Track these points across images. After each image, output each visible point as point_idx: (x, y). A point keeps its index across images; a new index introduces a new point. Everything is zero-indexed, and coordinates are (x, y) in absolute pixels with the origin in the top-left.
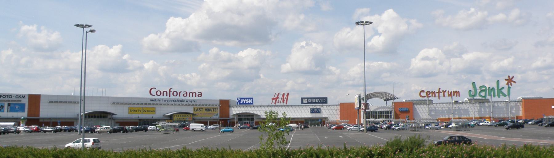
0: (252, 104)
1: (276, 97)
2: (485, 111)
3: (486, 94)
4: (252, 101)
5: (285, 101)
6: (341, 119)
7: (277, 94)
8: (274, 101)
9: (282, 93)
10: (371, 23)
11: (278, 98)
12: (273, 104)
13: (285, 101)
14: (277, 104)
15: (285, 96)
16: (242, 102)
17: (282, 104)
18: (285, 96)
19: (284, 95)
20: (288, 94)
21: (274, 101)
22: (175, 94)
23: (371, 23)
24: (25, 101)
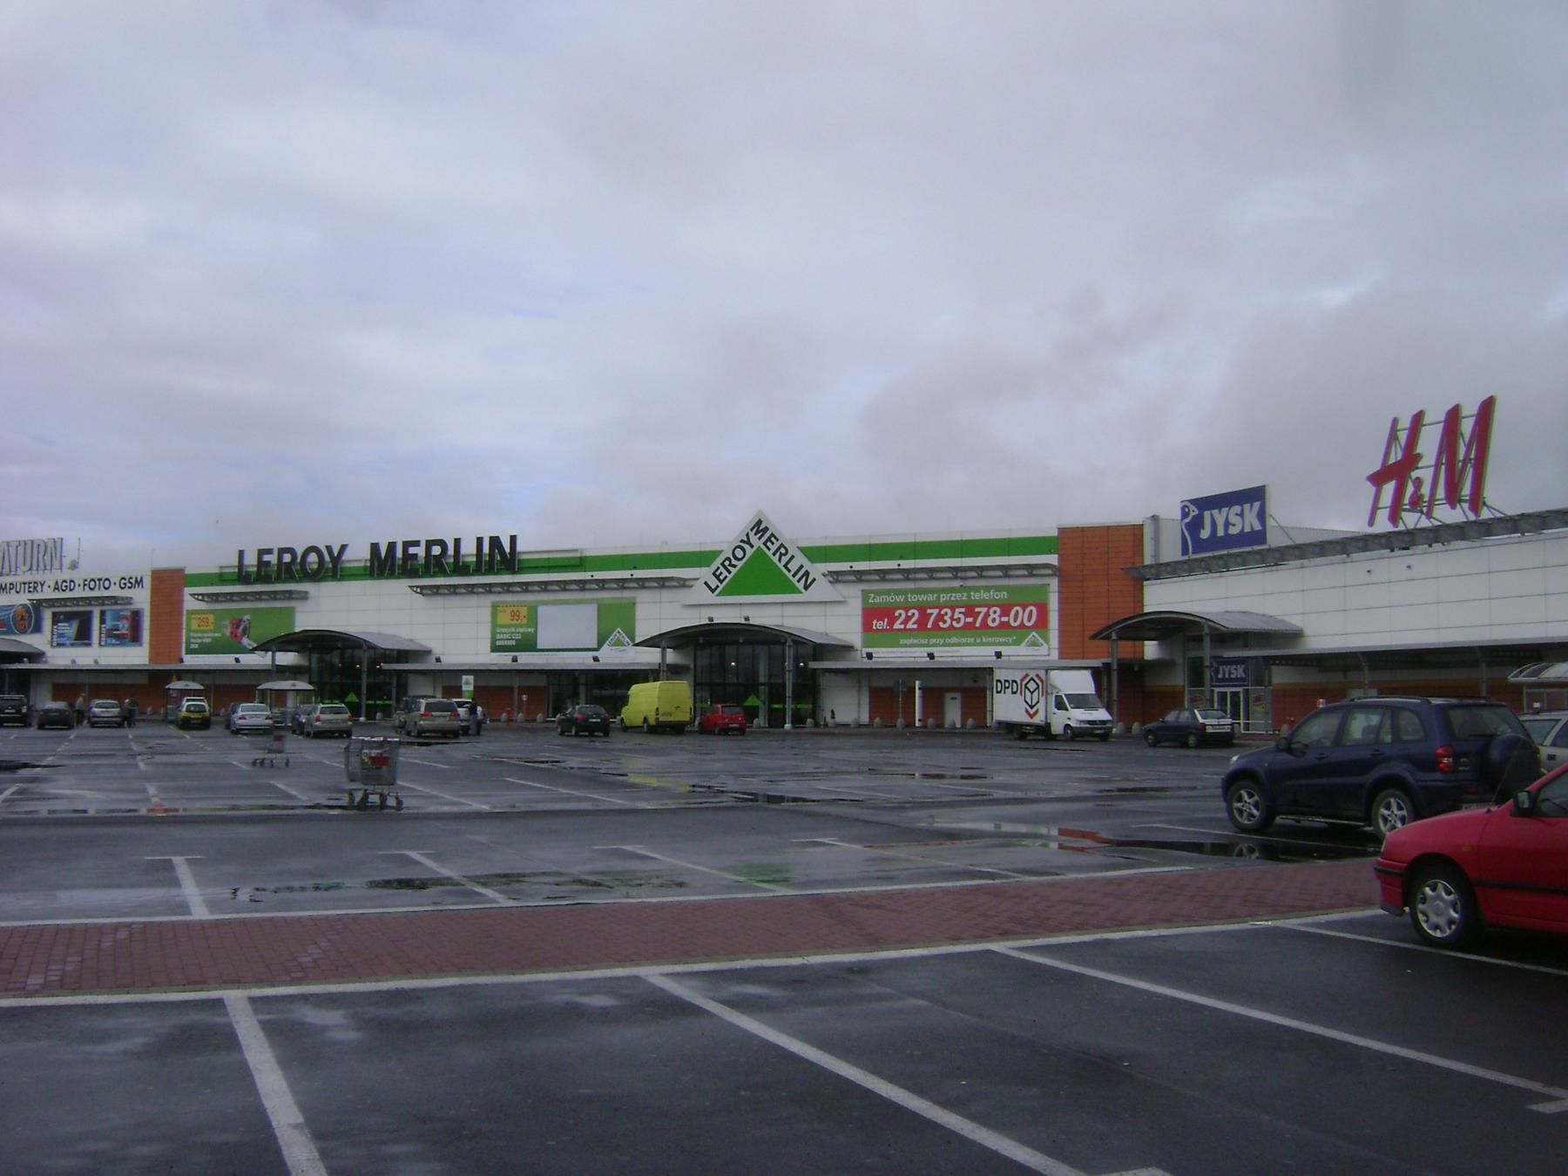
0: (1260, 536)
1: (1396, 455)
2: (1463, 765)
3: (461, 705)
4: (1262, 516)
5: (1466, 490)
6: (1061, 657)
7: (1405, 423)
8: (1389, 488)
9: (1436, 416)
10: (375, 885)
11: (1411, 459)
12: (1383, 525)
13: (1466, 490)
14: (1410, 520)
15: (1467, 427)
16: (1205, 534)
17: (1447, 515)
18: (1467, 427)
19: (1453, 416)
20: (1486, 411)
21: (1389, 488)
22: (739, 553)
23: (375, 885)
24: (142, 599)
